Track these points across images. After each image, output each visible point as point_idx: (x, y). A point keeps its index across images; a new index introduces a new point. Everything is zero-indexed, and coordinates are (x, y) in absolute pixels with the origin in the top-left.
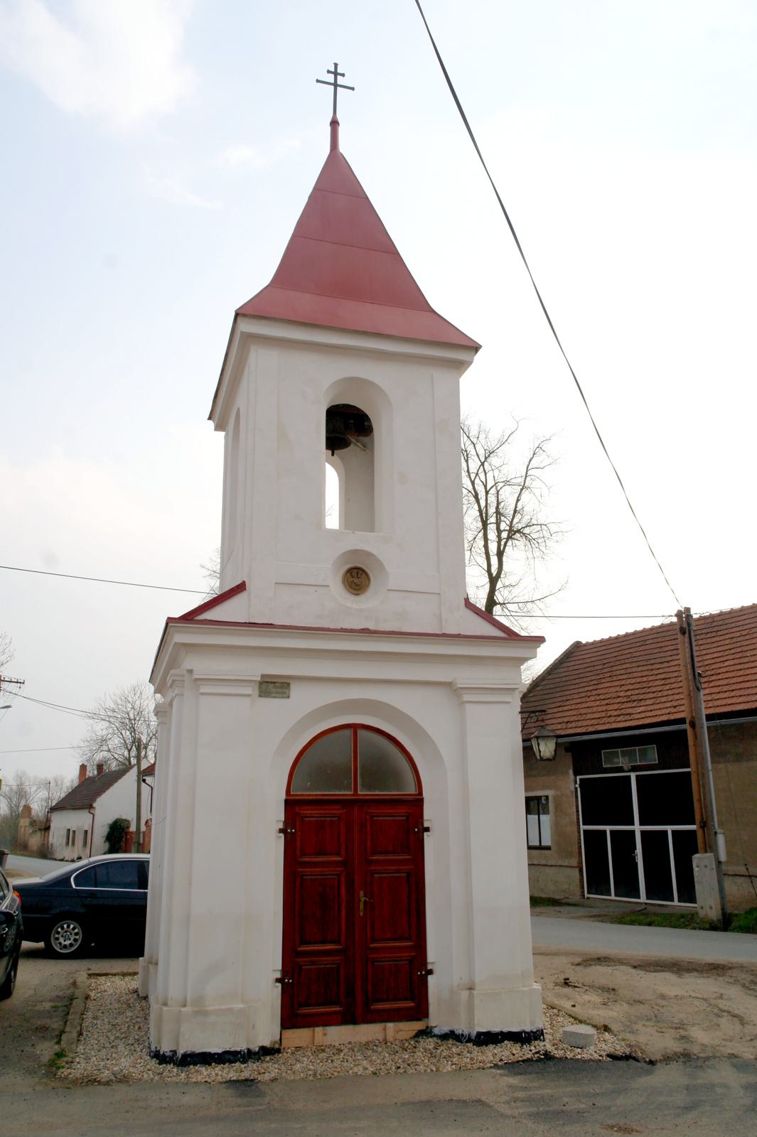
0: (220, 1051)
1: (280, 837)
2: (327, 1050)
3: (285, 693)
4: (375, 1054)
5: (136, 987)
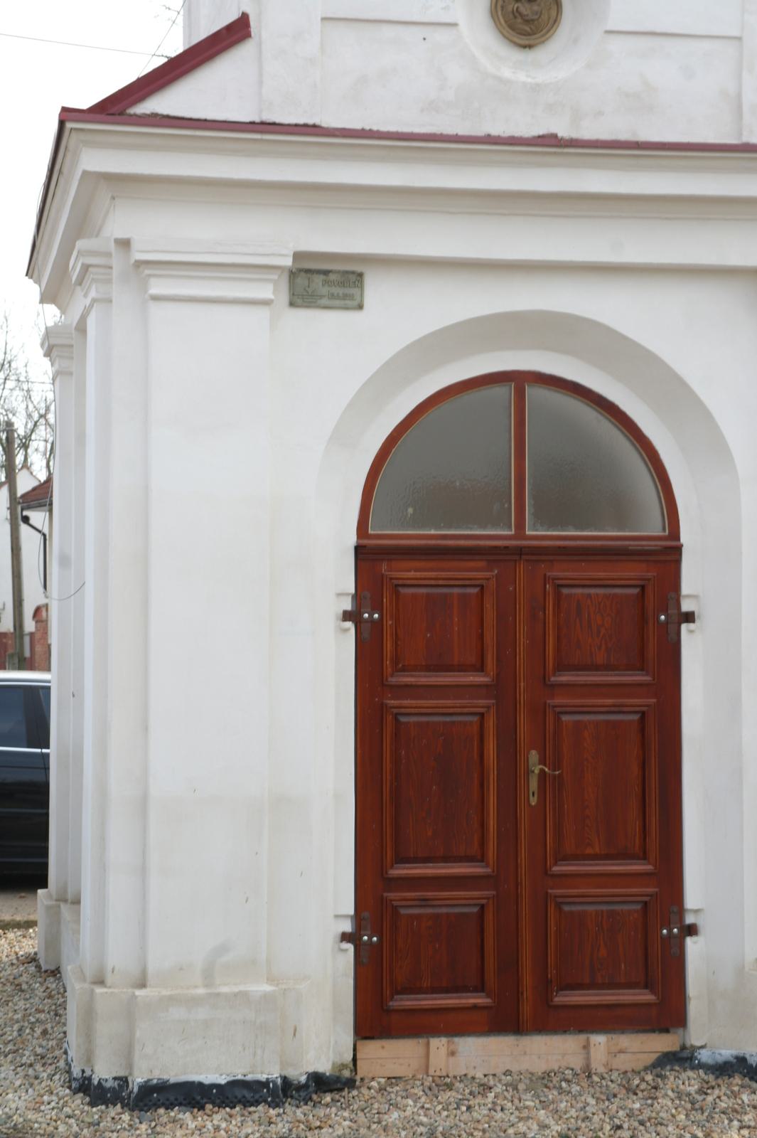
0: (222, 1080)
1: (347, 630)
2: (457, 1084)
3: (351, 297)
4: (565, 1098)
5: (32, 951)
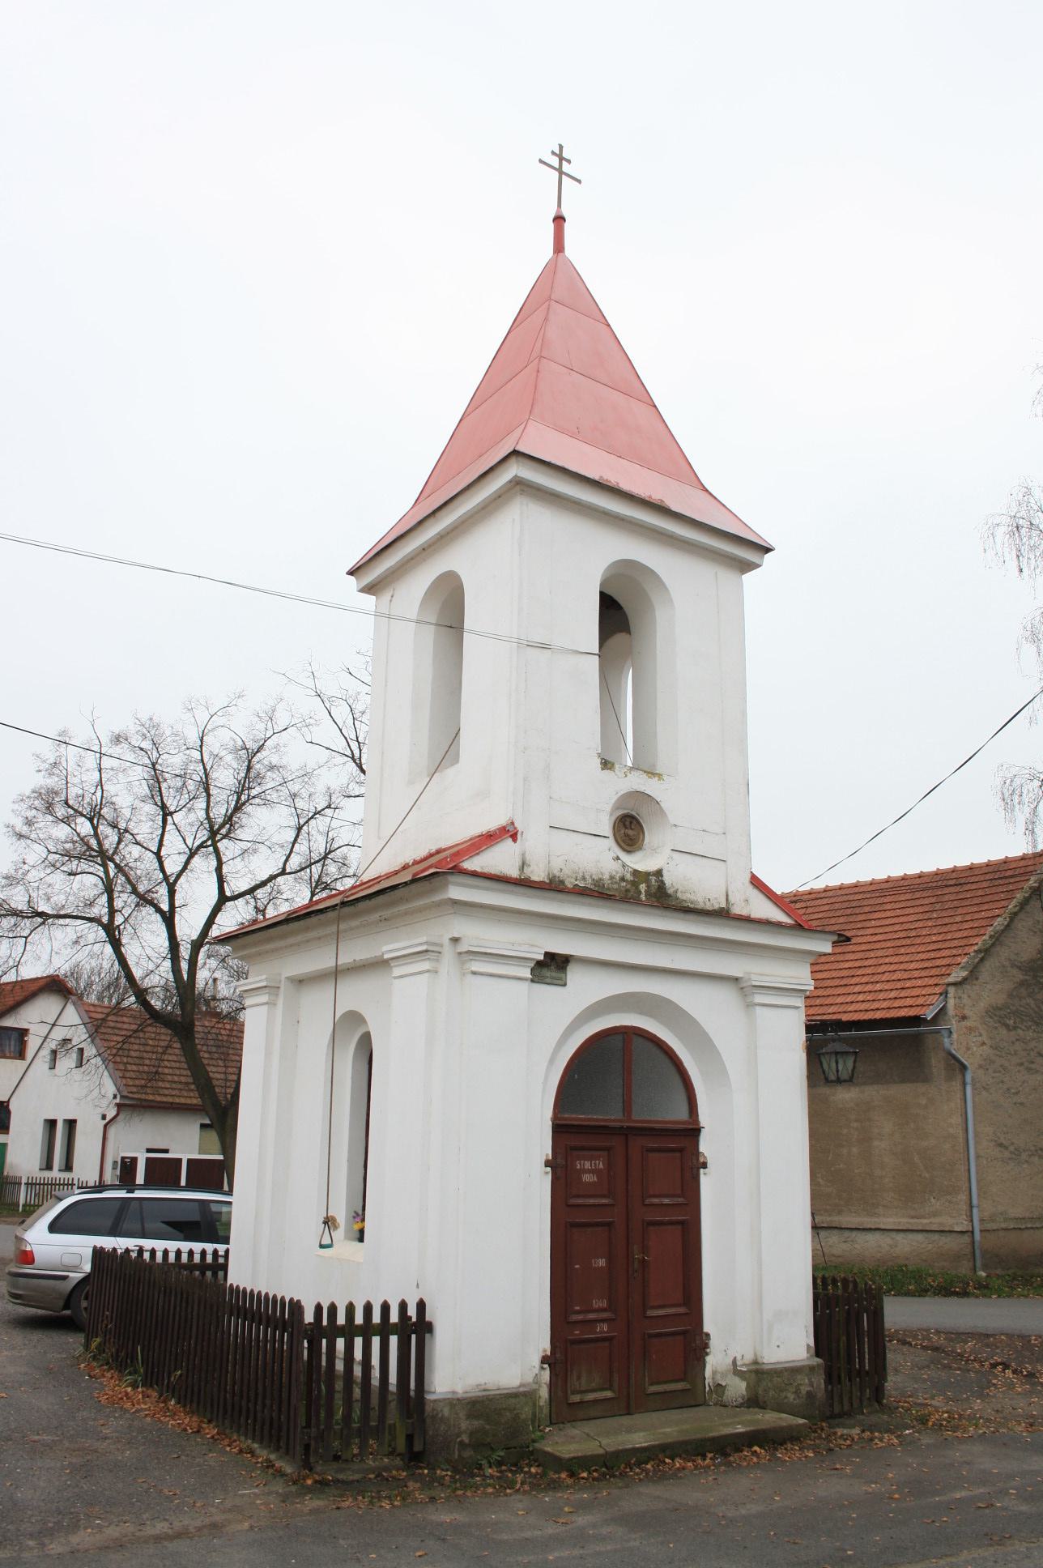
1: (547, 1173)
3: (561, 979)
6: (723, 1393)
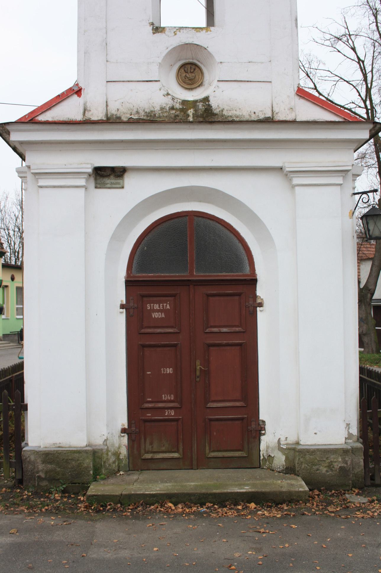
3: (119, 184)
6: (273, 462)
